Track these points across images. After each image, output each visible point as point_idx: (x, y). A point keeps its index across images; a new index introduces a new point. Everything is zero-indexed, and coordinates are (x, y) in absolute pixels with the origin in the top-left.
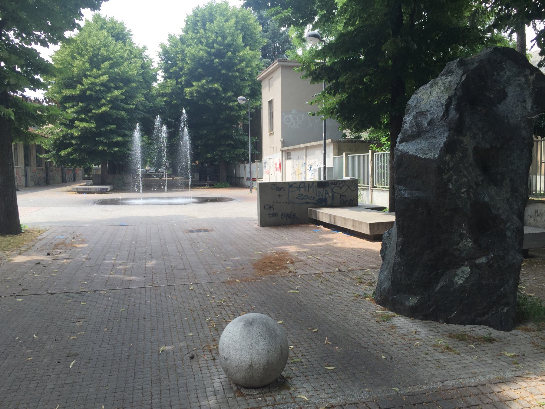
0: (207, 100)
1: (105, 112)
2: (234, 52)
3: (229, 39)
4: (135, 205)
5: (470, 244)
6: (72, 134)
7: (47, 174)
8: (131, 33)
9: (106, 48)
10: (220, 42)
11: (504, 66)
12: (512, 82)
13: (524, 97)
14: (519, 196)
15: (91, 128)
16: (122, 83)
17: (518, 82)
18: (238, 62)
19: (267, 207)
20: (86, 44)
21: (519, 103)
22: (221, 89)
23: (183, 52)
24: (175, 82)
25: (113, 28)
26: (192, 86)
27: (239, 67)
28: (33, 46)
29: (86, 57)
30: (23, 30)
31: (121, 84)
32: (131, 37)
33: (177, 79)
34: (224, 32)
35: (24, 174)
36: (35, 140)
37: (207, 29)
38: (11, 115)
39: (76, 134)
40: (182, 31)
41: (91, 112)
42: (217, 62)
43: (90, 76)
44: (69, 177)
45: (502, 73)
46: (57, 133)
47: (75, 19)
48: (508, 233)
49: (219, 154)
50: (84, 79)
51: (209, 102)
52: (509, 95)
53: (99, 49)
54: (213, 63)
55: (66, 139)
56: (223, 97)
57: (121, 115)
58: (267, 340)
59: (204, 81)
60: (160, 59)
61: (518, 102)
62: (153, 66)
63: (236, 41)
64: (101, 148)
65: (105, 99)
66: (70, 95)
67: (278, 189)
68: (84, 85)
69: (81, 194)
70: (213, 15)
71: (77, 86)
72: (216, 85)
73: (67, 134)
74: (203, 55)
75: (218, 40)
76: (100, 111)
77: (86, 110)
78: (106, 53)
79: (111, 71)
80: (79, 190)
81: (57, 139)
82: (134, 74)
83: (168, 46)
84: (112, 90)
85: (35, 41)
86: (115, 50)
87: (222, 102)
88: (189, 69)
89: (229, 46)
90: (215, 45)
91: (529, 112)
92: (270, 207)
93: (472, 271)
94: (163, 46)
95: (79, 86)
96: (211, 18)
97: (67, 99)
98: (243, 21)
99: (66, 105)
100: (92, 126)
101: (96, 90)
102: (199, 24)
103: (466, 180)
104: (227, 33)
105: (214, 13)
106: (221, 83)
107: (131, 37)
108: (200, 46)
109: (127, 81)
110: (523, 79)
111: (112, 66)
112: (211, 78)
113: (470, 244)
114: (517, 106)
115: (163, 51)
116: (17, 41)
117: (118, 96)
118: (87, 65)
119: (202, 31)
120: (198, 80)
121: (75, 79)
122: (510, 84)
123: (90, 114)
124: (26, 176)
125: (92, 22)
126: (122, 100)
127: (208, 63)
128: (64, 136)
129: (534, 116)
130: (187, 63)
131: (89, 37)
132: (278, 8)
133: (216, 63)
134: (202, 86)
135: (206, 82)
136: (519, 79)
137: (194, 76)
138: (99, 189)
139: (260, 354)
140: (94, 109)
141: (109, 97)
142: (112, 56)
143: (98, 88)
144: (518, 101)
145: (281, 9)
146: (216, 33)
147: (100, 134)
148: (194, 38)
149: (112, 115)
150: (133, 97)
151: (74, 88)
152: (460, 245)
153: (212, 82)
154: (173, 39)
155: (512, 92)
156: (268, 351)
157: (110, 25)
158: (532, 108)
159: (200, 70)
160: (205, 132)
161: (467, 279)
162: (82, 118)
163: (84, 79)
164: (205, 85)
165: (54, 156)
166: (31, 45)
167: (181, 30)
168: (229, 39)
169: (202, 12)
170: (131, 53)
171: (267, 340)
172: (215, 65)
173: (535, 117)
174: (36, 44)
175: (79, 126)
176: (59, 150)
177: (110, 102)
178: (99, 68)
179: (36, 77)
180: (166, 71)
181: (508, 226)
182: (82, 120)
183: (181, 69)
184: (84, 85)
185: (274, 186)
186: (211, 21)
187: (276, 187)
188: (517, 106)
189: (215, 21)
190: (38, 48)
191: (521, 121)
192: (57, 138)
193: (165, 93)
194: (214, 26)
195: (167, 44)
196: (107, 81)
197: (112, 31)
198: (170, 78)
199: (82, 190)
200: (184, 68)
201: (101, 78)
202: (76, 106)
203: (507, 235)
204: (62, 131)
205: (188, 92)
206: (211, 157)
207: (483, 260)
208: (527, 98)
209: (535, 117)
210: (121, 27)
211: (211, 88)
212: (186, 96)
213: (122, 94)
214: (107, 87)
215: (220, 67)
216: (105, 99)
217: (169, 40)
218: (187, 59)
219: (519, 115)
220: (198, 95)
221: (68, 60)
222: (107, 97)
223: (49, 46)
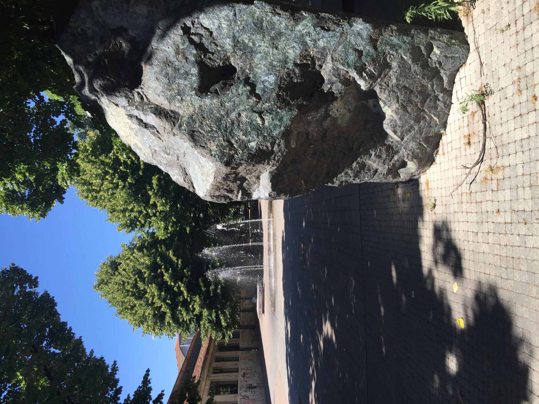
11: (79, 30)
12: (101, 20)
17: (100, 11)
35: (247, 352)
45: (89, 33)
61: (130, 11)
68: (162, 305)
77: (186, 304)
81: (212, 328)
90: (114, 181)
97: (174, 317)
99: (181, 321)
109: (154, 267)
111: (143, 280)
119: (101, 193)
135: (151, 190)
136: (95, 9)
138: (260, 294)
140: (184, 296)
144: (128, 11)
151: (165, 313)
153: (151, 184)
183: (140, 212)
188: (136, 13)
199: (261, 310)
216: (174, 286)
223: (120, 387)
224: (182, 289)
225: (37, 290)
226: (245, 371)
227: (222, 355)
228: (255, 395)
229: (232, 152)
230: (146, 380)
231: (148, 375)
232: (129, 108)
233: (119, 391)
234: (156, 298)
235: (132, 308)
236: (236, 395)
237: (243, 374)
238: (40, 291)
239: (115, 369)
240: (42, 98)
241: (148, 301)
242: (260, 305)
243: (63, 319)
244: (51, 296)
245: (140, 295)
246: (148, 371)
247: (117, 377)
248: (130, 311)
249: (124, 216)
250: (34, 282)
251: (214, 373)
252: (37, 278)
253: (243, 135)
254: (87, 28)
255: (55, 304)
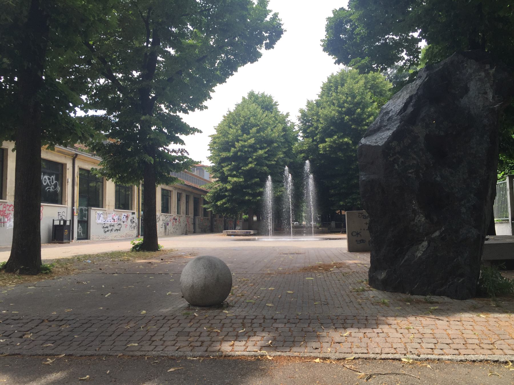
0: (338, 153)
1: (251, 168)
2: (363, 109)
3: (358, 98)
4: (264, 241)
5: (423, 219)
6: (226, 188)
7: (212, 224)
8: (277, 104)
9: (255, 117)
10: (350, 101)
11: (466, 65)
13: (485, 90)
14: (478, 177)
15: (240, 182)
16: (266, 144)
17: (479, 77)
18: (367, 117)
19: (354, 234)
20: (240, 115)
21: (480, 95)
22: (351, 142)
23: (317, 114)
24: (311, 140)
25: (263, 102)
26: (326, 142)
27: (367, 121)
28: (178, 113)
29: (239, 126)
30: (170, 103)
31: (265, 145)
32: (277, 107)
33: (313, 138)
34: (354, 92)
36: (174, 182)
37: (339, 91)
38: (151, 161)
39: (229, 187)
40: (319, 96)
41: (241, 169)
42: (347, 119)
43: (241, 140)
44: (231, 227)
46: (216, 188)
47: (210, 91)
48: (463, 210)
49: (351, 201)
50: (236, 143)
51: (340, 154)
52: (470, 90)
53: (249, 118)
54: (344, 120)
55: (222, 192)
56: (353, 149)
57: (264, 170)
58: (206, 270)
59: (336, 137)
60: (299, 122)
62: (295, 129)
63: (365, 98)
64: (247, 198)
65: (252, 158)
66: (226, 157)
67: (364, 218)
68: (236, 148)
69: (229, 236)
70: (344, 80)
71: (231, 149)
72: (346, 140)
73: (223, 189)
74: (335, 114)
75: (348, 100)
76: (247, 168)
77: (237, 168)
78: (254, 121)
79: (258, 135)
80: (228, 234)
81: (215, 192)
82: (276, 136)
83: (306, 111)
84: (258, 150)
85: (179, 110)
86: (262, 118)
87: (352, 154)
88: (322, 128)
89: (357, 105)
90: (345, 104)
91: (491, 102)
92: (358, 234)
93: (429, 245)
94: (302, 111)
95: (233, 149)
96: (343, 82)
98: (373, 81)
100: (241, 180)
101: (245, 151)
102: (332, 89)
103: (415, 162)
104: (357, 93)
105: (345, 78)
106: (351, 138)
107: (277, 107)
108: (332, 107)
109: (270, 142)
110: (483, 74)
111: (258, 131)
112: (342, 134)
113: (423, 219)
114: (478, 98)
115: (302, 115)
116: (167, 111)
117: (262, 155)
118: (239, 132)
119: (334, 94)
120: (331, 136)
121: (230, 144)
122: (472, 80)
123: (240, 171)
124: (194, 224)
125: (248, 98)
126: (266, 158)
127: (340, 120)
128: (220, 190)
129: (496, 105)
130: (321, 123)
131: (243, 110)
132: (358, 58)
133: (346, 120)
134: (334, 142)
135: (338, 137)
136: (480, 74)
137: (327, 133)
138: (244, 232)
139: (199, 278)
140: (243, 166)
141: (254, 156)
142: (259, 123)
143: (246, 149)
145: (361, 59)
146: (347, 94)
147: (247, 187)
148: (328, 101)
149: (257, 170)
150: (274, 155)
151: (229, 151)
152: (416, 221)
153: (343, 137)
154: (311, 105)
155: (473, 86)
156: (206, 277)
157: (261, 99)
158: (493, 97)
159: (332, 128)
160: (338, 182)
161: (424, 252)
162: (234, 174)
163: (236, 143)
164: (337, 140)
165: (212, 206)
166: (176, 113)
167: (318, 96)
168: (358, 98)
169: (335, 78)
170: (276, 120)
171: (206, 270)
172: (345, 121)
173: (497, 106)
174: (180, 112)
175: (231, 181)
176: (217, 202)
177: (256, 160)
178: (248, 134)
179: (177, 135)
180: (304, 131)
181: (463, 204)
182: (234, 176)
183: (317, 128)
184: (236, 148)
185: (361, 215)
186: (342, 85)
187: (363, 215)
188: (478, 98)
189: (345, 84)
190: (181, 114)
191: (482, 110)
192: (215, 192)
193: (303, 150)
194: (345, 89)
195: (305, 108)
196: (254, 143)
197: (262, 104)
198: (307, 137)
199: (231, 233)
200: (319, 128)
201: (249, 141)
202: (231, 165)
203: (462, 212)
204: (219, 186)
205: (322, 147)
206: (343, 204)
207: (437, 234)
208: (488, 90)
209: (497, 106)
210: (269, 100)
211: (342, 142)
212: (320, 151)
213: (265, 153)
214: (254, 148)
215: (350, 123)
216: (252, 158)
217: (307, 106)
218: (320, 119)
219: (481, 106)
220: (330, 149)
221: (226, 130)
222: (253, 156)
224: (250, 165)
225: (263, 49)
226: (178, 220)
227: (191, 201)
228: (160, 227)
229: (391, 155)
230: (194, 130)
231: (198, 132)
232: (416, 96)
233: (185, 112)
234: (243, 143)
235: (235, 124)
236: (161, 212)
237: (176, 218)
238: (262, 50)
239: (202, 108)
240: (420, 40)
241: (240, 136)
242: (235, 232)
243: (239, 69)
244: (259, 59)
245: (245, 130)
246: (201, 132)
247: (196, 109)
248: (232, 122)
249: (313, 115)
250: (269, 46)
251: (178, 193)
252: (273, 48)
253: (402, 161)
254: (467, 70)
255: (252, 62)
